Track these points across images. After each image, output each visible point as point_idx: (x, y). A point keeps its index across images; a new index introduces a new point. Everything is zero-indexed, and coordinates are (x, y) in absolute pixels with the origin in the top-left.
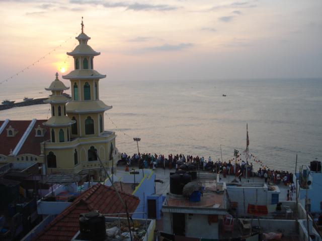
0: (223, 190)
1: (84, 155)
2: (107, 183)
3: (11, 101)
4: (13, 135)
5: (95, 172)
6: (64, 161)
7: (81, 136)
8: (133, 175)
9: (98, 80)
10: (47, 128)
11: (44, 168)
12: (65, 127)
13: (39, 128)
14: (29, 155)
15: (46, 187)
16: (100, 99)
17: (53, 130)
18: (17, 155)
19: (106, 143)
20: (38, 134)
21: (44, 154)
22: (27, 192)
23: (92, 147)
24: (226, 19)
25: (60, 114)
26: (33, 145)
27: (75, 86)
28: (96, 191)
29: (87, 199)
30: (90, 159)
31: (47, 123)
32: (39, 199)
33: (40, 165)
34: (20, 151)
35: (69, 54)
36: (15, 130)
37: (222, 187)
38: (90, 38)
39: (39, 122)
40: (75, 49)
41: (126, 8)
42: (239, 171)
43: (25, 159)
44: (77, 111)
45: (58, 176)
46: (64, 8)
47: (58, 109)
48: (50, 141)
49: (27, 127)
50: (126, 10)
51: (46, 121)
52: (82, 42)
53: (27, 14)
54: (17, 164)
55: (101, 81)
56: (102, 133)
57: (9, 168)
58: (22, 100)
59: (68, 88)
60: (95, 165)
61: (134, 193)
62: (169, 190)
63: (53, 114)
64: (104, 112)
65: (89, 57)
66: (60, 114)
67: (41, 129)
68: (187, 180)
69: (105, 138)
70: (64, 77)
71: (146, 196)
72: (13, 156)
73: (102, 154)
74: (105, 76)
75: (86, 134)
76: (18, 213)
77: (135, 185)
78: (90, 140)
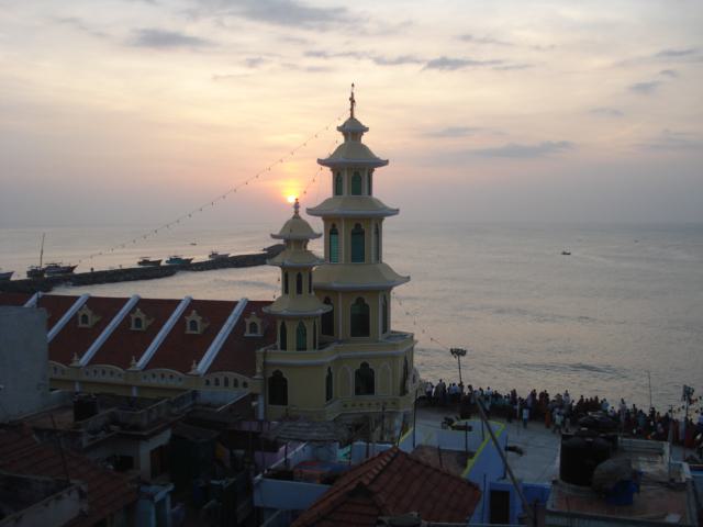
0: (684, 480)
1: (346, 383)
2: (405, 444)
3: (184, 258)
4: (90, 325)
5: (366, 417)
6: (305, 394)
7: (340, 338)
8: (463, 433)
9: (382, 220)
10: (271, 319)
11: (260, 404)
12: (309, 318)
13: (254, 318)
14: (232, 376)
15: (273, 447)
16: (385, 260)
17: (283, 323)
18: (207, 372)
19: (394, 357)
20: (191, 329)
21: (264, 373)
22: (232, 454)
23: (365, 365)
24: (643, 88)
25: (299, 290)
26: (239, 355)
27: (332, 231)
28: (389, 464)
29: (373, 482)
30: (358, 392)
31: (273, 309)
32: (257, 474)
33: (253, 397)
34: (92, 359)
35: (321, 162)
36: (203, 321)
37: (679, 473)
38: (367, 130)
39: (252, 306)
40: (335, 153)
41: (422, 66)
42: (699, 437)
43: (222, 381)
44: (335, 285)
45: (300, 425)
46: (292, 67)
47: (296, 279)
48: (276, 348)
49: (228, 315)
50: (424, 69)
51: (269, 303)
52: (350, 138)
53: (216, 78)
54: (207, 394)
55: (387, 223)
56: (387, 334)
57: (191, 403)
58: (204, 258)
59: (320, 236)
60: (104, 373)
61: (465, 474)
62: (558, 472)
63: (286, 290)
64: (390, 288)
65: (364, 169)
66: (299, 290)
67: (258, 322)
68: (602, 455)
69: (394, 345)
70: (310, 212)
71: (488, 480)
72: (198, 376)
73: (385, 383)
74: (396, 212)
75: (353, 335)
76: (213, 502)
77: (464, 456)
78: (360, 350)
